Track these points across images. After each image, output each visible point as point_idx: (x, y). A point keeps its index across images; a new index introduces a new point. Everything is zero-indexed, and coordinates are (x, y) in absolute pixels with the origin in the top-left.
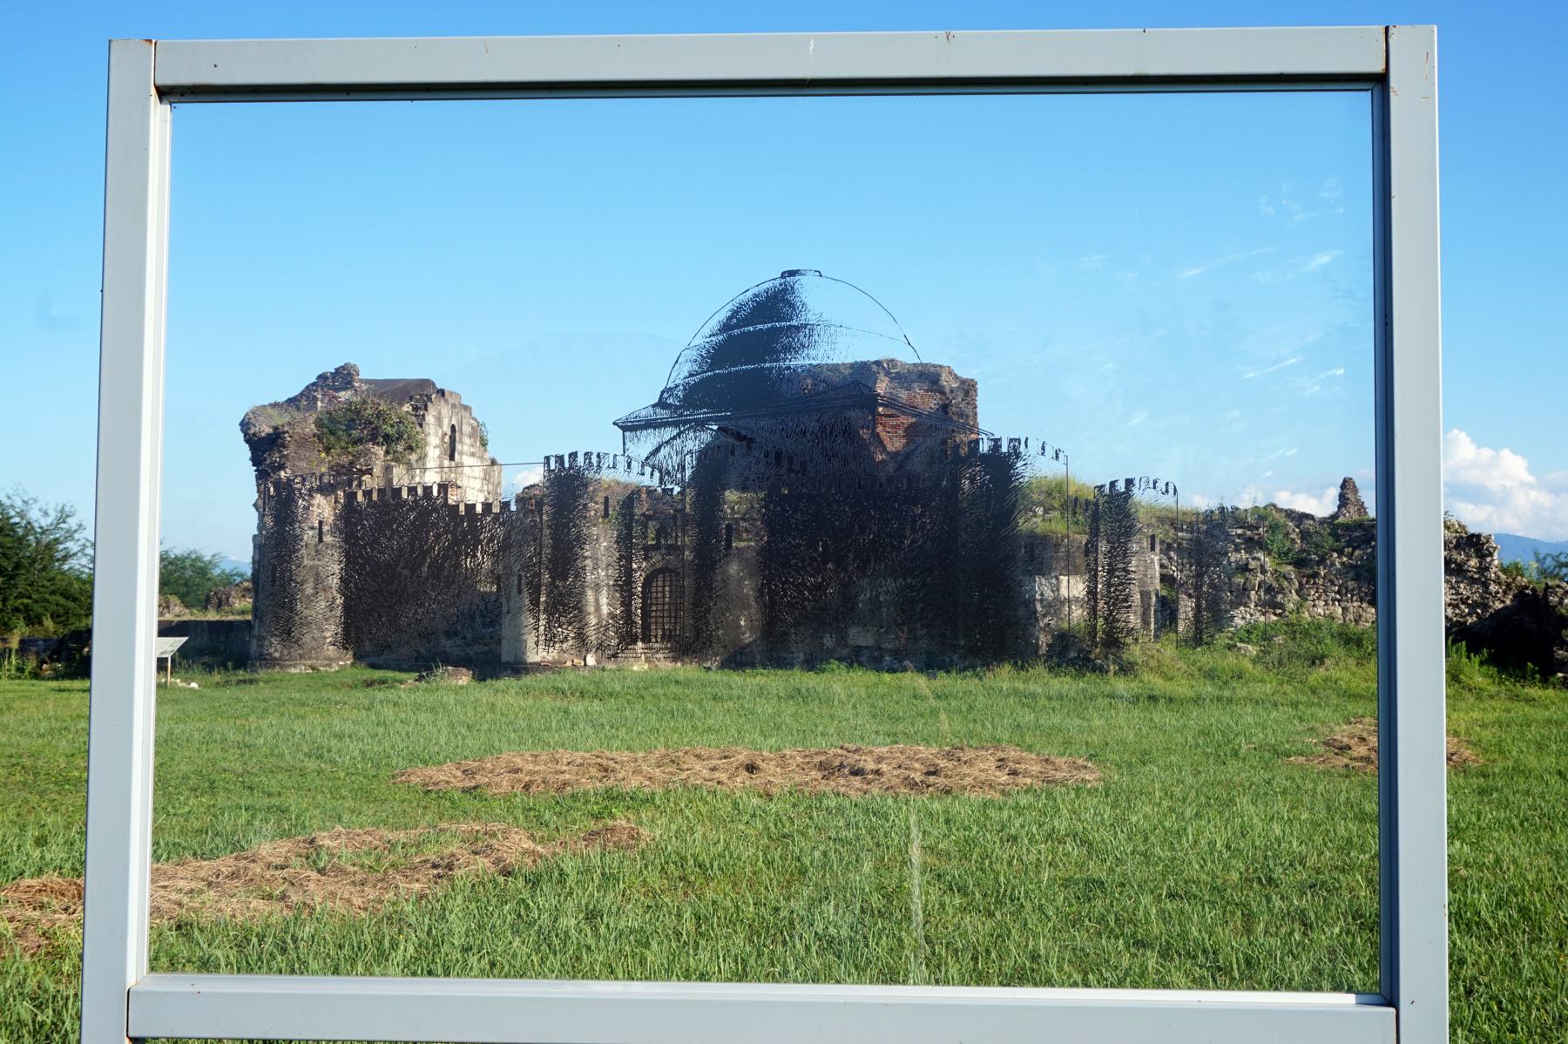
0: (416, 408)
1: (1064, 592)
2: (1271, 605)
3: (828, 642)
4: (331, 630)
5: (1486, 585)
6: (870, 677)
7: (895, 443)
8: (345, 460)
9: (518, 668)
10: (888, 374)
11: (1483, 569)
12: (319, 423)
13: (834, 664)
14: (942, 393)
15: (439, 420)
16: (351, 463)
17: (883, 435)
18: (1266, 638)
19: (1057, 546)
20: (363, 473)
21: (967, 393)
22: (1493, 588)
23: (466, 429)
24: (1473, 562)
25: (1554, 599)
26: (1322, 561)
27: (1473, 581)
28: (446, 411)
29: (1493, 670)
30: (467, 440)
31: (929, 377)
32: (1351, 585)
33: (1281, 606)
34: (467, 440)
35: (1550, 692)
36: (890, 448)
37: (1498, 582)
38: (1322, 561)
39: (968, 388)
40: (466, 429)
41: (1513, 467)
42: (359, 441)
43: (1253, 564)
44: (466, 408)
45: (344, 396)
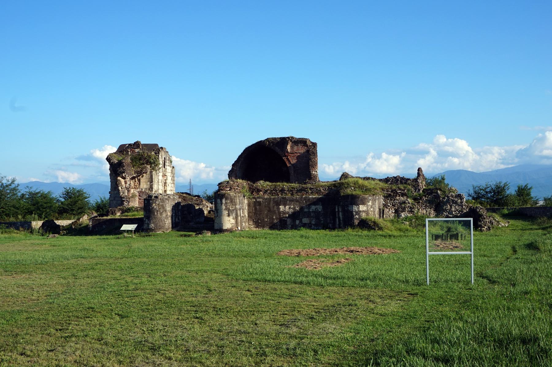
0: (156, 153)
1: (361, 209)
2: (411, 212)
3: (297, 222)
4: (168, 222)
5: (462, 206)
6: (327, 232)
7: (294, 161)
8: (139, 169)
9: (221, 230)
10: (291, 141)
11: (462, 202)
12: (132, 159)
13: (302, 228)
14: (307, 146)
15: (162, 156)
16: (141, 171)
17: (290, 159)
18: (411, 220)
19: (359, 197)
20: (144, 173)
21: (314, 147)
22: (464, 207)
23: (167, 158)
24: (459, 201)
25: (478, 210)
26: (421, 199)
27: (459, 205)
28: (163, 153)
29: (464, 227)
30: (168, 162)
31: (303, 142)
32: (428, 205)
33: (413, 212)
34: (168, 162)
35: (477, 232)
36: (292, 163)
37: (465, 205)
38: (421, 199)
39: (314, 145)
40: (167, 158)
41: (462, 145)
42: (143, 164)
43: (407, 202)
44: (167, 152)
45: (137, 150)
